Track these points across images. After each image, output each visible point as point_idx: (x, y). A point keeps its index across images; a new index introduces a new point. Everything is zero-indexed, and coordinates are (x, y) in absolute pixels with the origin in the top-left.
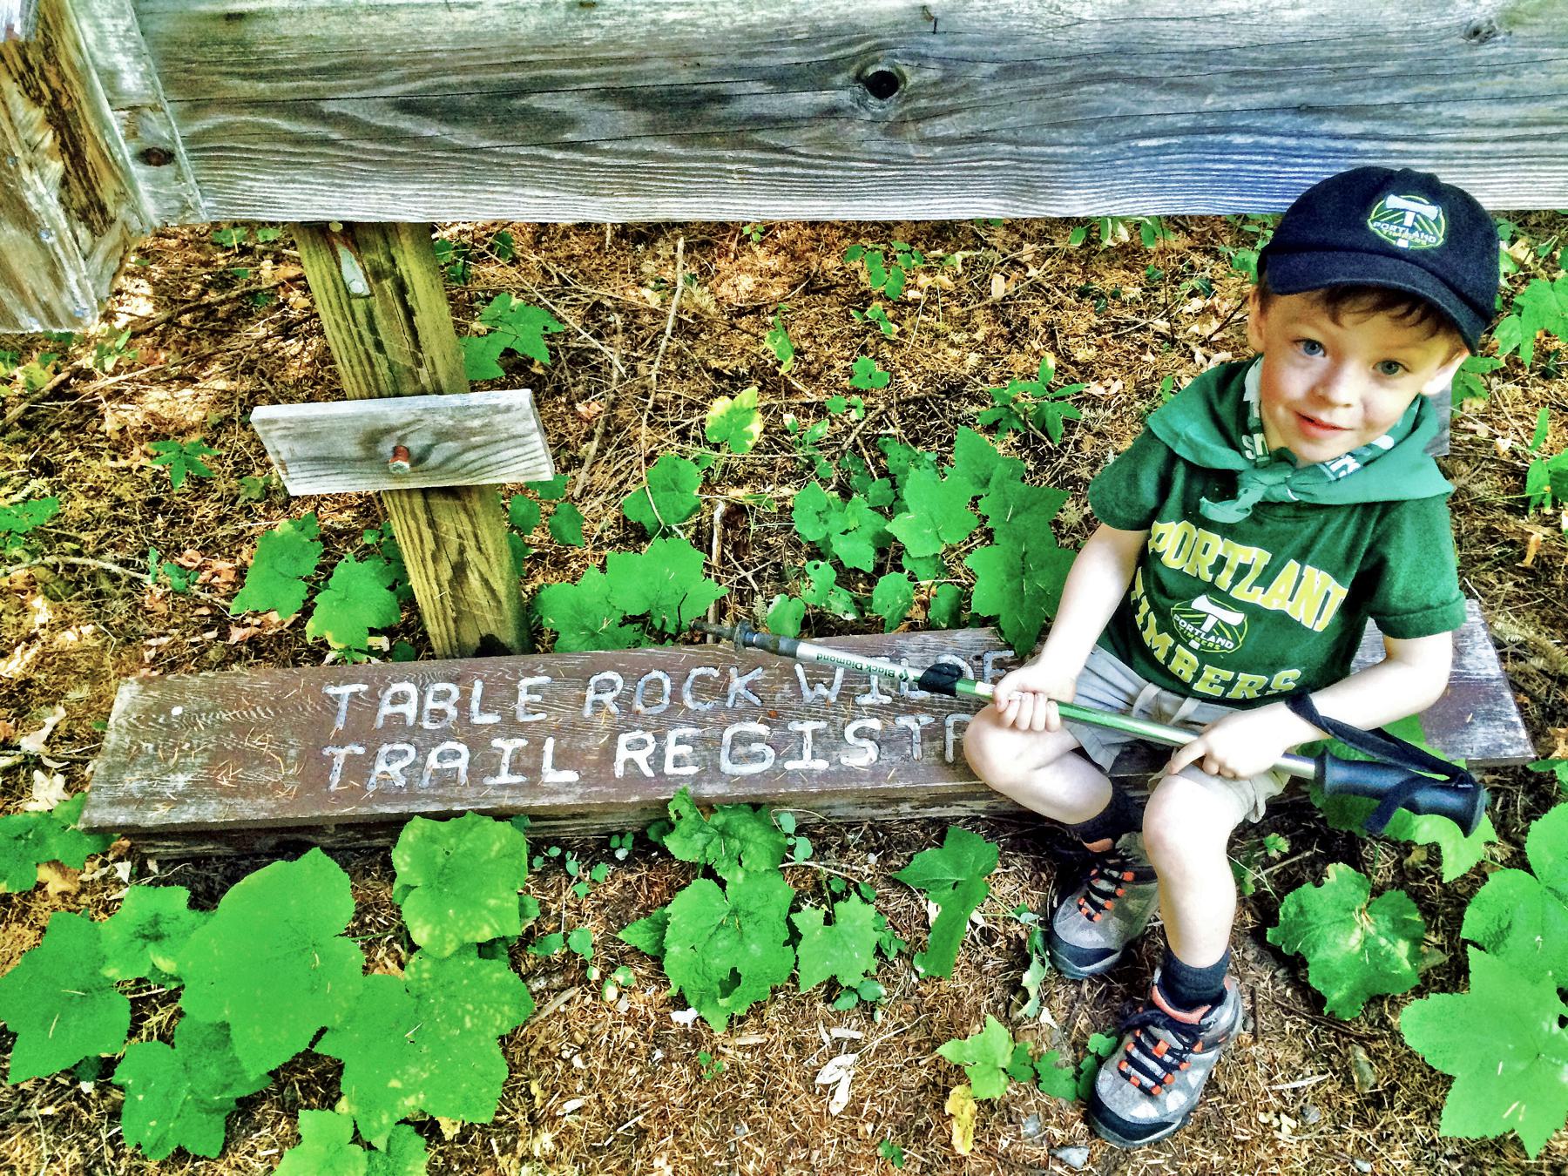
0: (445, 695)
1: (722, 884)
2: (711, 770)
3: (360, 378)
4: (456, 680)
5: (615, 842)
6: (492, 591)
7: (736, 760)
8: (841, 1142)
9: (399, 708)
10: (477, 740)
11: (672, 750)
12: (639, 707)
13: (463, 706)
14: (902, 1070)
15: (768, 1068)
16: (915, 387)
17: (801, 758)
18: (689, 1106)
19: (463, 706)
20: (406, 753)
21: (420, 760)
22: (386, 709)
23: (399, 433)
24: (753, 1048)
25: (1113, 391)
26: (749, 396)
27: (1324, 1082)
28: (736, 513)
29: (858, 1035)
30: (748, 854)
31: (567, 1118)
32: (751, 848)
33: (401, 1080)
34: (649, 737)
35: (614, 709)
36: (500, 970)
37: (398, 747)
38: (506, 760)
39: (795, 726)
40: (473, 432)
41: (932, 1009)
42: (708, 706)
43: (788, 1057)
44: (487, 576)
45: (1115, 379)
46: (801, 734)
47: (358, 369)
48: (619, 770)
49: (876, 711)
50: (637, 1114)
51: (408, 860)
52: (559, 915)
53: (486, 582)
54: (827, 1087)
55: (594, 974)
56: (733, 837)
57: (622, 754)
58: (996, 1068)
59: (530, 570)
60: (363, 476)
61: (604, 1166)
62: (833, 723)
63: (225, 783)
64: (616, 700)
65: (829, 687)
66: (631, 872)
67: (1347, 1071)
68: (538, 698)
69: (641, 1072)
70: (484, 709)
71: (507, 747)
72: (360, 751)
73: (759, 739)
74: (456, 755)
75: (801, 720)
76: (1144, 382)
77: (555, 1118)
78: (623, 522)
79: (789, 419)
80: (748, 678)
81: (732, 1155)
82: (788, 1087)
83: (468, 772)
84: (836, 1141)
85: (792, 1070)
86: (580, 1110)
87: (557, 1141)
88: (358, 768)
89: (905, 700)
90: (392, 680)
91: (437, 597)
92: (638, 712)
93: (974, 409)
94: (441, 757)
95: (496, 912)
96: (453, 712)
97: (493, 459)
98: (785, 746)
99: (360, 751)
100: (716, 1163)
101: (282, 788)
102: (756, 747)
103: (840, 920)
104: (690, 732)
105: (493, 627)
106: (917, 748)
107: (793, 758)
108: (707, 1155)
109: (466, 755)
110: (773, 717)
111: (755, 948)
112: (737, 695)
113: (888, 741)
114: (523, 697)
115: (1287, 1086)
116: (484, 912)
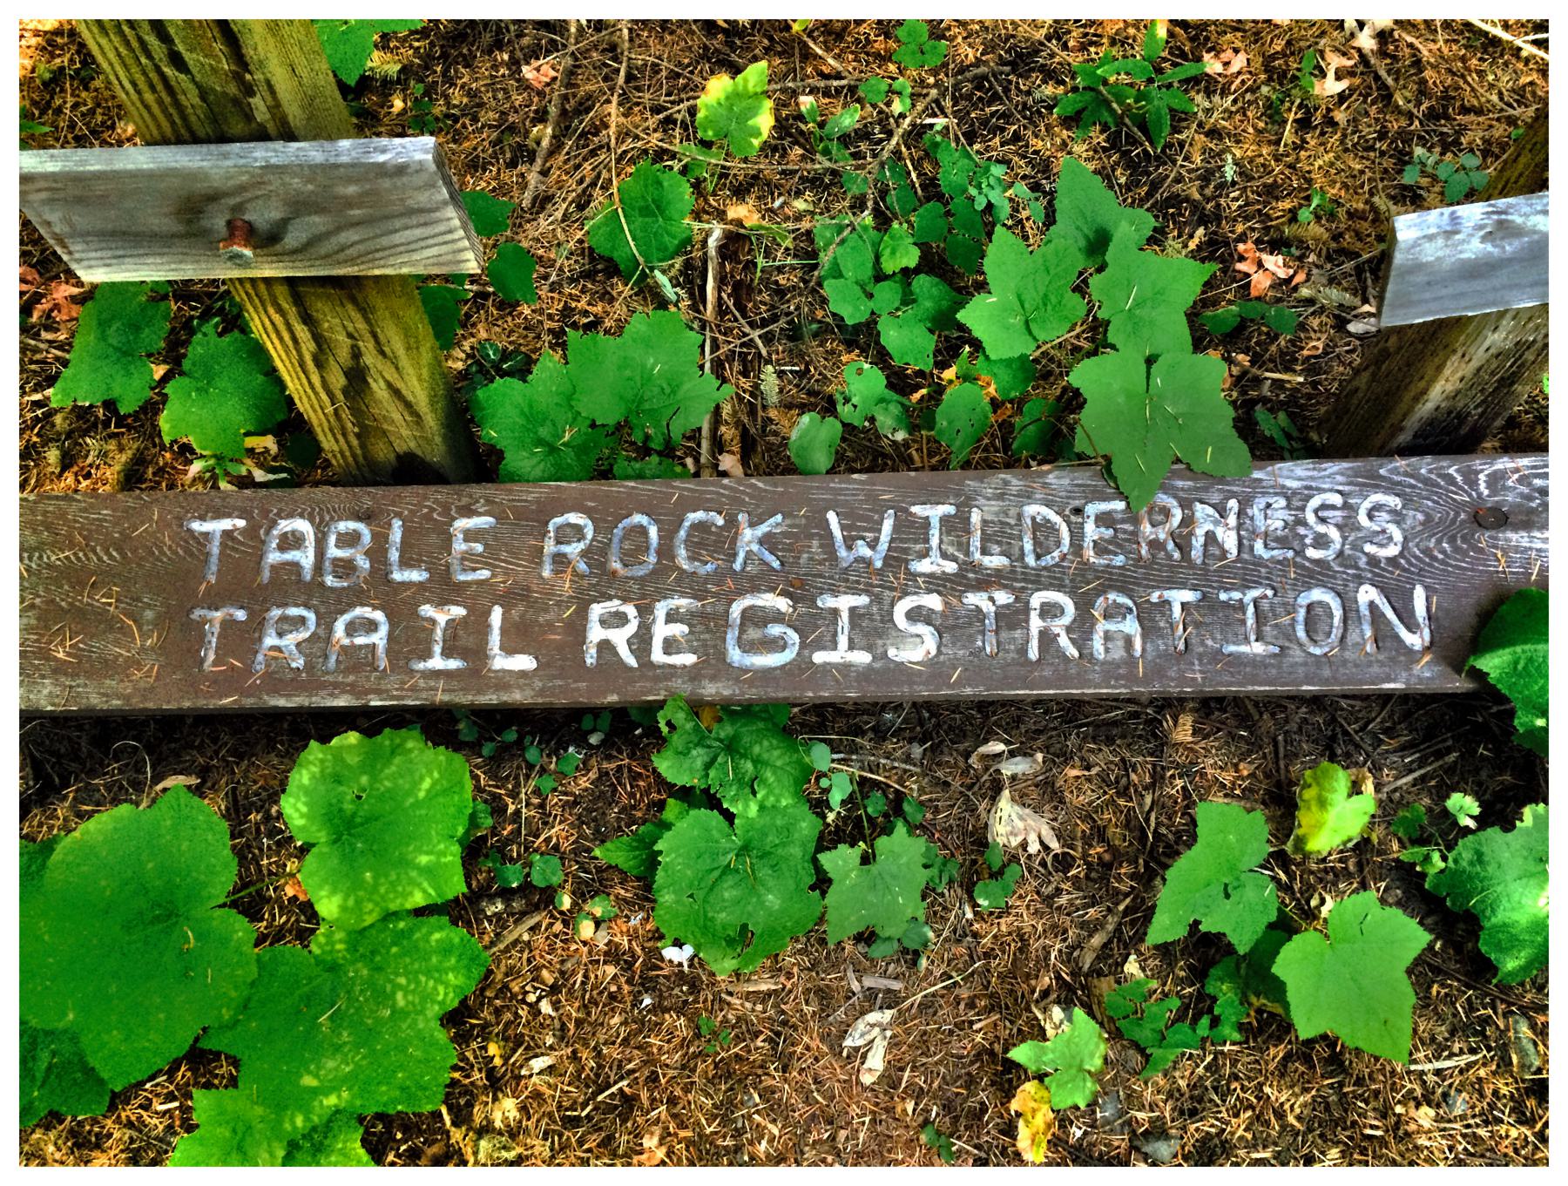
0: (350, 540)
1: (729, 817)
2: (713, 662)
3: (156, 109)
4: (366, 517)
5: (587, 723)
6: (408, 405)
7: (748, 647)
8: (873, 1121)
9: (291, 556)
10: (400, 605)
11: (661, 630)
12: (616, 565)
13: (377, 553)
14: (951, 1032)
15: (785, 1023)
16: (970, 52)
17: (835, 648)
18: (686, 1067)
19: (377, 553)
20: (302, 621)
21: (321, 632)
22: (274, 557)
23: (232, 201)
24: (764, 997)
25: (1234, 69)
26: (756, 74)
27: (1475, 1062)
28: (735, 242)
29: (897, 985)
30: (764, 782)
31: (535, 1079)
32: (769, 775)
33: (317, 1076)
34: (630, 610)
35: (582, 567)
36: (441, 928)
37: (294, 611)
38: (438, 635)
39: (826, 601)
40: (349, 203)
41: (987, 955)
42: (709, 567)
43: (808, 1009)
44: (399, 385)
45: (1236, 51)
46: (835, 612)
47: (149, 97)
48: (591, 658)
49: (936, 583)
50: (622, 1078)
51: (304, 809)
52: (518, 812)
53: (396, 393)
54: (857, 1049)
55: (566, 902)
56: (744, 756)
57: (596, 633)
58: (1081, 1069)
59: (468, 316)
60: (184, 257)
61: (581, 1142)
62: (877, 599)
63: (61, 655)
64: (584, 554)
65: (873, 545)
66: (609, 758)
67: (1504, 1049)
68: (479, 548)
69: (625, 1023)
70: (405, 563)
71: (441, 616)
72: (241, 615)
73: (778, 617)
74: (372, 626)
75: (835, 592)
76: (1273, 57)
77: (519, 1078)
78: (587, 252)
79: (806, 102)
80: (763, 529)
81: (738, 1133)
82: (808, 1048)
83: (388, 651)
84: (867, 1119)
85: (814, 1025)
86: (551, 1069)
87: (523, 1109)
88: (242, 639)
89: (976, 568)
90: (279, 516)
91: (330, 410)
92: (614, 573)
93: (1049, 90)
94: (351, 629)
95: (429, 872)
96: (363, 563)
97: (385, 241)
98: (816, 628)
99: (241, 615)
100: (719, 1142)
101: (139, 665)
102: (775, 630)
103: (881, 858)
104: (683, 603)
105: (412, 445)
106: (991, 638)
107: (824, 648)
108: (708, 1131)
109: (384, 630)
110: (800, 591)
111: (772, 900)
112: (749, 554)
113: (954, 627)
114: (459, 546)
115: (1428, 1067)
116: (414, 874)
